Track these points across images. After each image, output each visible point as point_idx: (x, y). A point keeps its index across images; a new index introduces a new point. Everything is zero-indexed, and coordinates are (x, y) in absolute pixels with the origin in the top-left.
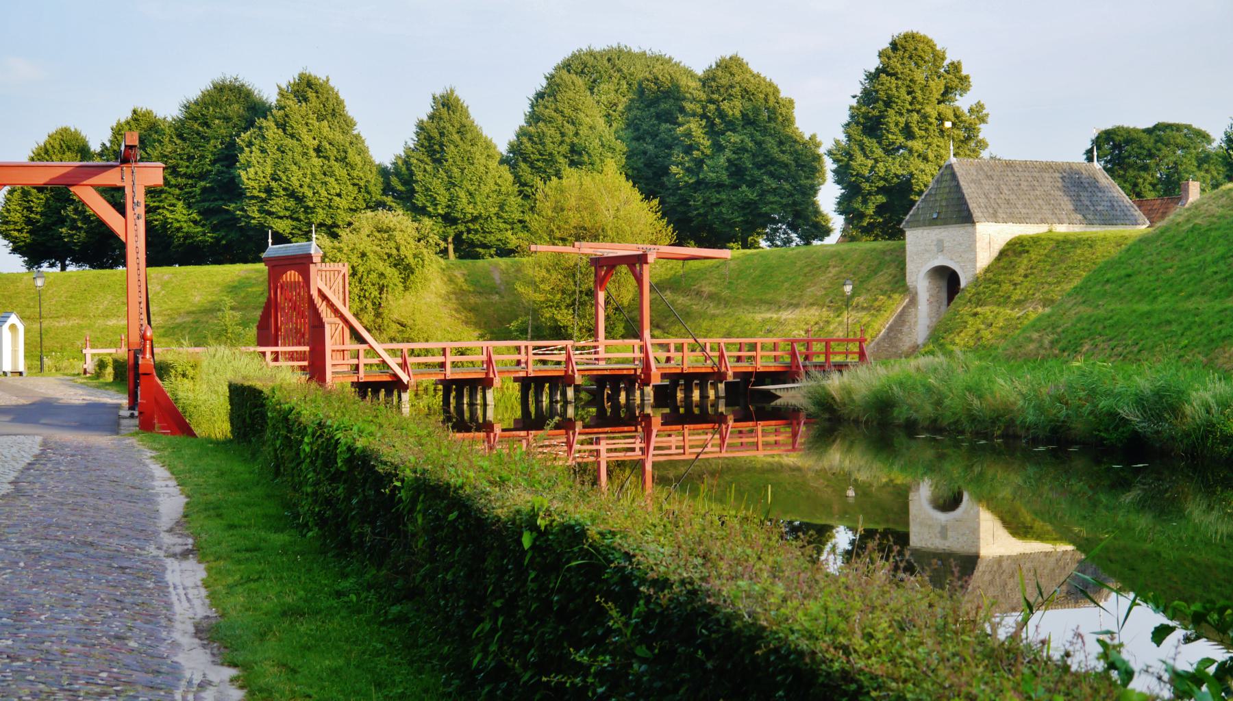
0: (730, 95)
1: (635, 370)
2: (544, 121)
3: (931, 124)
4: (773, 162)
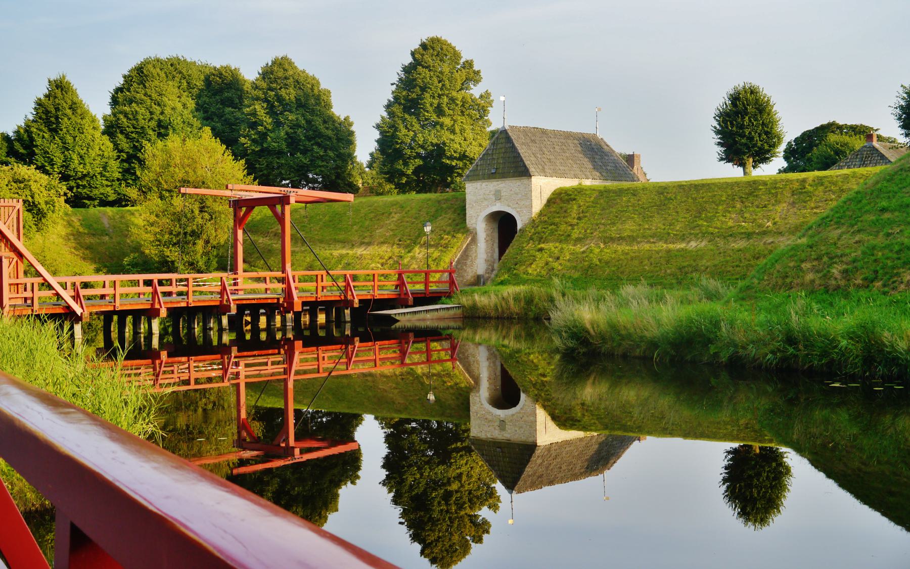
0: (286, 85)
1: (278, 299)
2: (136, 102)
3: (457, 105)
4: (320, 135)
